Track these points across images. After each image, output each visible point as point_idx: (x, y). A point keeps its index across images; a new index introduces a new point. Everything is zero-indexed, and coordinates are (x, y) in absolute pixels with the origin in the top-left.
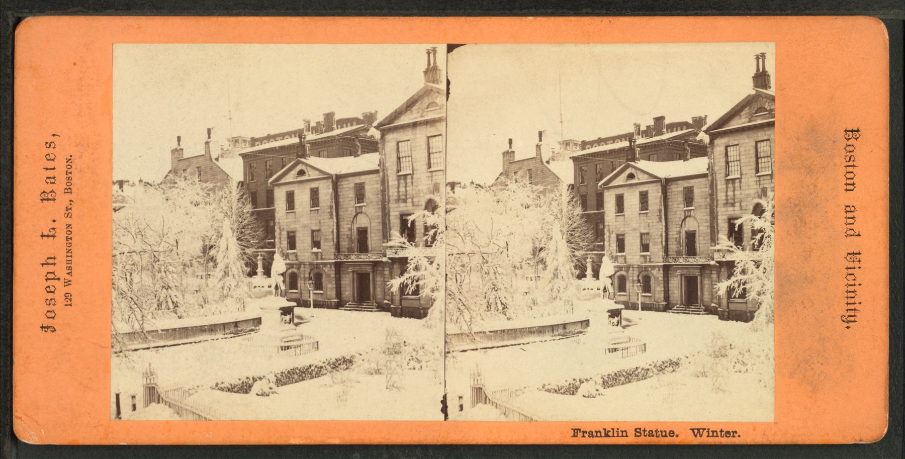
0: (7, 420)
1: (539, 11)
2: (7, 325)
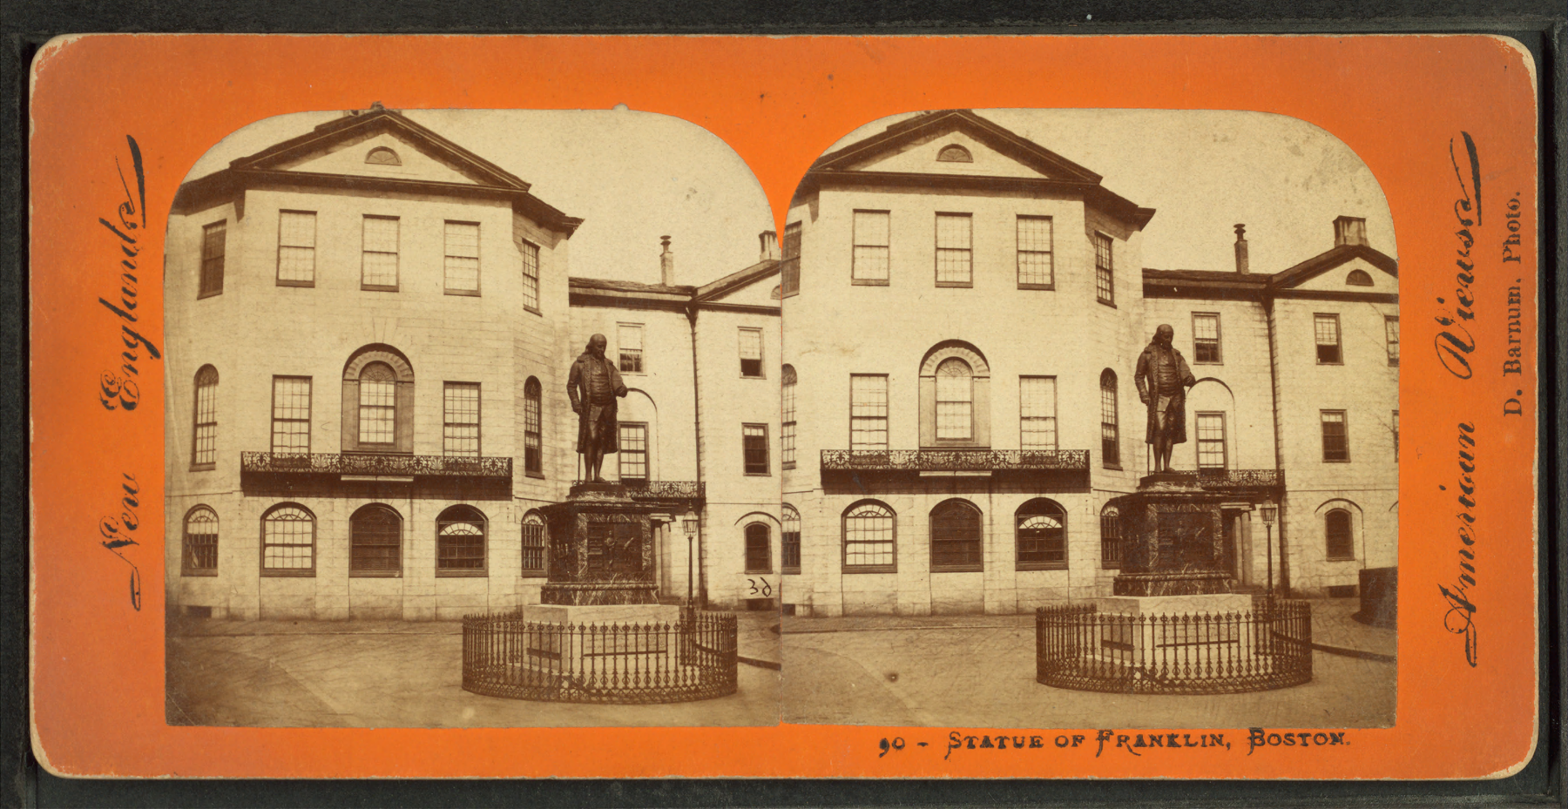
1: (920, 23)
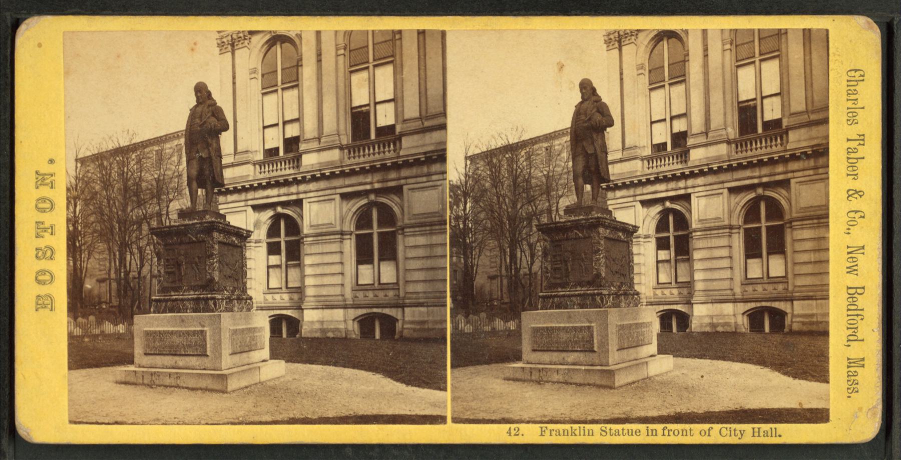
0: (5, 414)
2: (6, 320)
